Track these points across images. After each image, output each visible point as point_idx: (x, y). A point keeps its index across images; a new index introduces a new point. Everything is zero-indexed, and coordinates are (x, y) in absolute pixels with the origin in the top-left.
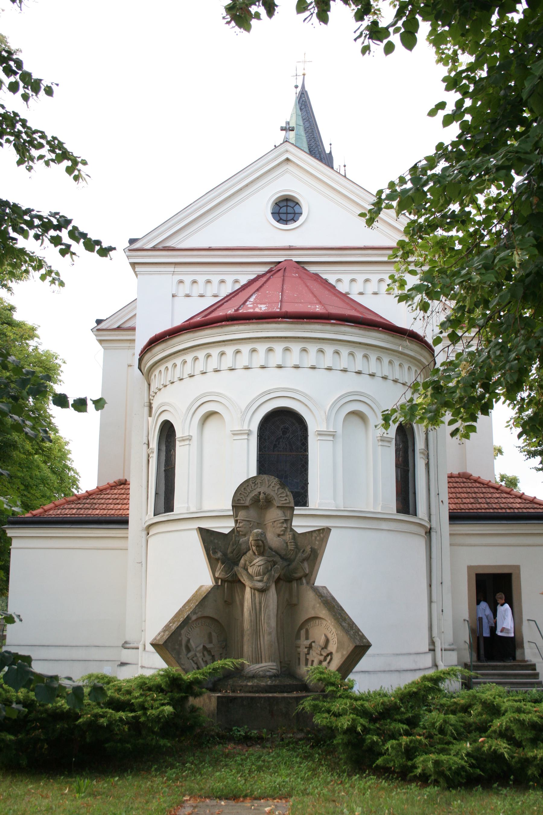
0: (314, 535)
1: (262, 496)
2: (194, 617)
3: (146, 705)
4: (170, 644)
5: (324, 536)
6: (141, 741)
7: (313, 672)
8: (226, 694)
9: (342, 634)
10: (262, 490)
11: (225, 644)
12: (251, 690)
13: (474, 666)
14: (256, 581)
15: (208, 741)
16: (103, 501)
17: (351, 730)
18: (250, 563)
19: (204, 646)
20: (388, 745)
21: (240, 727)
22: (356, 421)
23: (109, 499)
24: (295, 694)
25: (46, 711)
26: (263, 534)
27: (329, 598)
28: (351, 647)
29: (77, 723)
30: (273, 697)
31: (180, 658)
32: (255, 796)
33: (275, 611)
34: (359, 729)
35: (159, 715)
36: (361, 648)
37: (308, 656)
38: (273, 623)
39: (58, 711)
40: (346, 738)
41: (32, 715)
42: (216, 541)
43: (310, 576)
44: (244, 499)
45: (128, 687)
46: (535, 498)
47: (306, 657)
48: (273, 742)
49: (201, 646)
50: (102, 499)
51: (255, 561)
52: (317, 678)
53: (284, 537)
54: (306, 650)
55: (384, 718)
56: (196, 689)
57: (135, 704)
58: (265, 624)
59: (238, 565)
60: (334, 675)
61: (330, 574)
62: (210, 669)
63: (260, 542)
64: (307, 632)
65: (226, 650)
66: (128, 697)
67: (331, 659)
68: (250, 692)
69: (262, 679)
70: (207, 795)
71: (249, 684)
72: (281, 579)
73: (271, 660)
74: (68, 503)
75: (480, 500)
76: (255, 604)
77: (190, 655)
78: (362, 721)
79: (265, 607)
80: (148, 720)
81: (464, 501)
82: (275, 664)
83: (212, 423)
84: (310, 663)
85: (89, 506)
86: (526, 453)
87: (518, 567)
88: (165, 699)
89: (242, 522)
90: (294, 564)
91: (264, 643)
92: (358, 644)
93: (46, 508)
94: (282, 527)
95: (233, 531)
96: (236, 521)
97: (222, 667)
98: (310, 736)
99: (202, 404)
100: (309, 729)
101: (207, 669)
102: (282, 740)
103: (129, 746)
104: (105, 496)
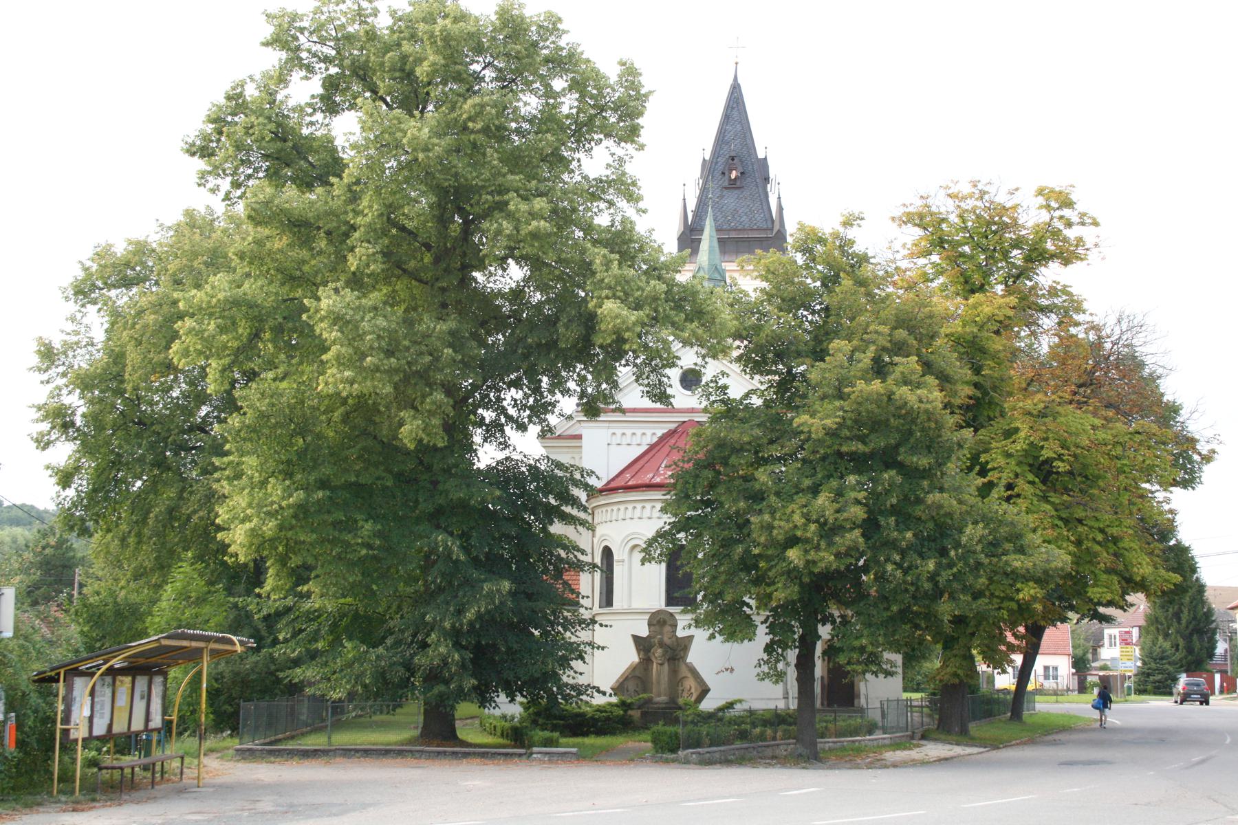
4: (618, 689)
36: (705, 691)
43: (684, 658)
61: (693, 657)
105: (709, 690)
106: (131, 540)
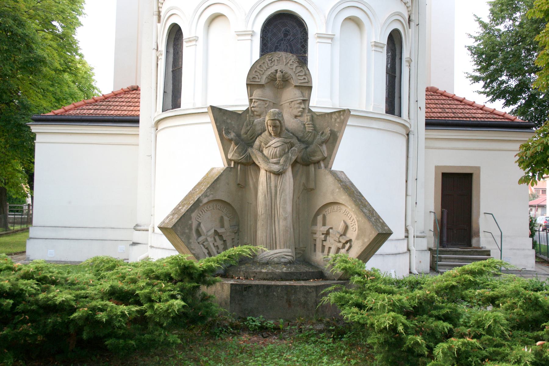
0: (334, 116)
1: (279, 74)
2: (205, 200)
3: (153, 298)
4: (179, 228)
5: (345, 118)
6: (147, 336)
8: (239, 282)
9: (363, 220)
10: (279, 68)
12: (265, 277)
13: (440, 251)
14: (272, 163)
15: (221, 332)
16: (117, 104)
17: (393, 329)
18: (266, 144)
19: (215, 231)
22: (352, 26)
23: (123, 102)
25: (37, 302)
28: (376, 234)
29: (72, 317)
30: (291, 286)
31: (190, 243)
34: (400, 328)
35: (168, 310)
38: (289, 208)
39: (49, 302)
40: (381, 337)
41: (20, 307)
43: (327, 160)
44: (260, 77)
45: (133, 274)
46: (495, 109)
47: (323, 243)
48: (290, 333)
49: (213, 231)
50: (116, 102)
51: (271, 143)
52: (342, 267)
53: (301, 119)
54: (323, 236)
56: (209, 278)
58: (281, 209)
59: (252, 146)
62: (225, 256)
63: (277, 122)
65: (238, 235)
66: (132, 286)
67: (350, 247)
68: (264, 279)
69: (277, 265)
72: (298, 163)
74: (86, 104)
75: (447, 110)
76: (270, 187)
77: (201, 239)
79: (281, 191)
81: (433, 110)
82: (290, 250)
83: (217, 25)
85: (104, 107)
86: (471, 79)
87: (478, 168)
88: (174, 290)
90: (312, 147)
91: (279, 228)
92: (380, 231)
93: (68, 108)
94: (299, 108)
96: (251, 100)
99: (208, 6)
100: (328, 319)
101: (222, 256)
103: (133, 342)
104: (120, 100)
106: (419, 286)
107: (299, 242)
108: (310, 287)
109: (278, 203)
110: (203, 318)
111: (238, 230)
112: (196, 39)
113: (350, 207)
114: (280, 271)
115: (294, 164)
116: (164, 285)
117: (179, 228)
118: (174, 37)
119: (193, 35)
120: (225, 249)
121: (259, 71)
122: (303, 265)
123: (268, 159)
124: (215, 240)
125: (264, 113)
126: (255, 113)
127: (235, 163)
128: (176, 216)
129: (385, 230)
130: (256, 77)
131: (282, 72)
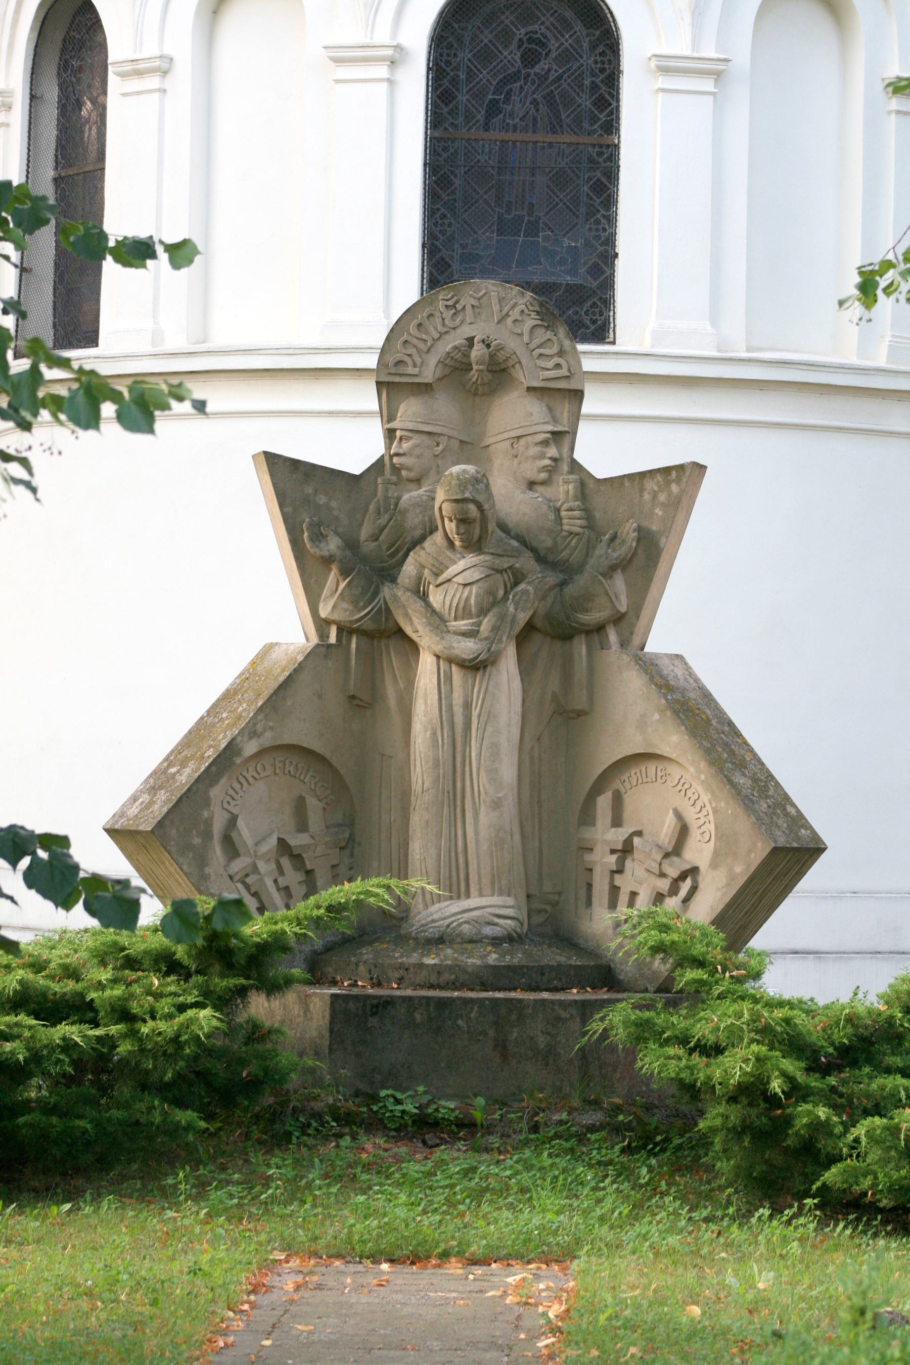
0: (650, 485)
1: (477, 352)
2: (251, 748)
5: (682, 492)
7: (635, 927)
9: (730, 808)
10: (478, 331)
11: (347, 835)
12: (433, 979)
15: (304, 1128)
17: (752, 1091)
18: (437, 575)
19: (281, 841)
20: (860, 1130)
21: (404, 1092)
24: (574, 994)
26: (481, 481)
27: (692, 695)
28: (760, 852)
31: (205, 877)
32: (473, 1254)
33: (516, 732)
35: (178, 1036)
36: (791, 857)
37: (617, 876)
38: (508, 771)
40: (735, 1114)
42: (322, 499)
43: (629, 622)
44: (418, 361)
47: (612, 880)
49: (273, 841)
52: (650, 943)
53: (548, 491)
54: (613, 858)
55: (855, 1064)
57: (97, 1003)
59: (394, 580)
60: (704, 935)
61: (696, 617)
62: (319, 907)
63: (472, 507)
64: (618, 801)
65: (352, 855)
66: (70, 986)
67: (694, 889)
68: (432, 987)
69: (469, 946)
70: (333, 1251)
71: (430, 961)
73: (497, 888)
76: (450, 707)
77: (238, 865)
78: (790, 1065)
80: (142, 1050)
82: (510, 901)
84: (623, 898)
89: (408, 439)
90: (581, 582)
91: (477, 833)
92: (782, 842)
94: (542, 456)
95: (378, 466)
96: (390, 434)
97: (357, 901)
98: (621, 1117)
100: (617, 1100)
101: (305, 907)
102: (535, 1128)
105: (812, 850)
107: (540, 874)
108: (563, 1004)
109: (473, 754)
110: (254, 1086)
111: (351, 839)
112: (164, 68)
113: (692, 770)
114: (479, 962)
115: (525, 636)
116: (156, 982)
117: (174, 831)
118: (59, 36)
119: (150, 49)
120: (312, 890)
121: (415, 341)
122: (550, 946)
123: (443, 620)
124: (281, 870)
125: (432, 472)
126: (404, 473)
127: (340, 630)
128: (162, 795)
129: (798, 838)
130: (407, 359)
131: (488, 346)
